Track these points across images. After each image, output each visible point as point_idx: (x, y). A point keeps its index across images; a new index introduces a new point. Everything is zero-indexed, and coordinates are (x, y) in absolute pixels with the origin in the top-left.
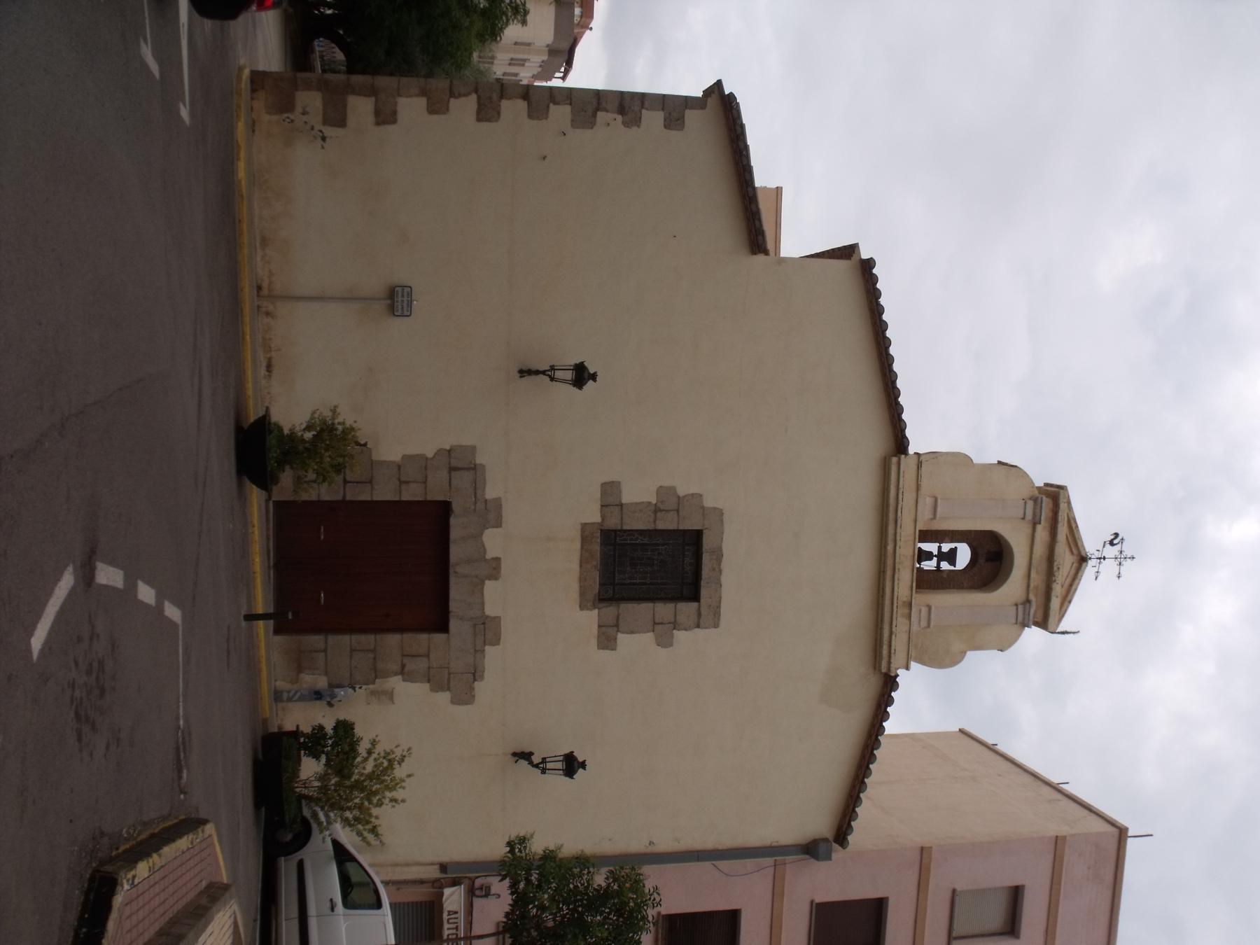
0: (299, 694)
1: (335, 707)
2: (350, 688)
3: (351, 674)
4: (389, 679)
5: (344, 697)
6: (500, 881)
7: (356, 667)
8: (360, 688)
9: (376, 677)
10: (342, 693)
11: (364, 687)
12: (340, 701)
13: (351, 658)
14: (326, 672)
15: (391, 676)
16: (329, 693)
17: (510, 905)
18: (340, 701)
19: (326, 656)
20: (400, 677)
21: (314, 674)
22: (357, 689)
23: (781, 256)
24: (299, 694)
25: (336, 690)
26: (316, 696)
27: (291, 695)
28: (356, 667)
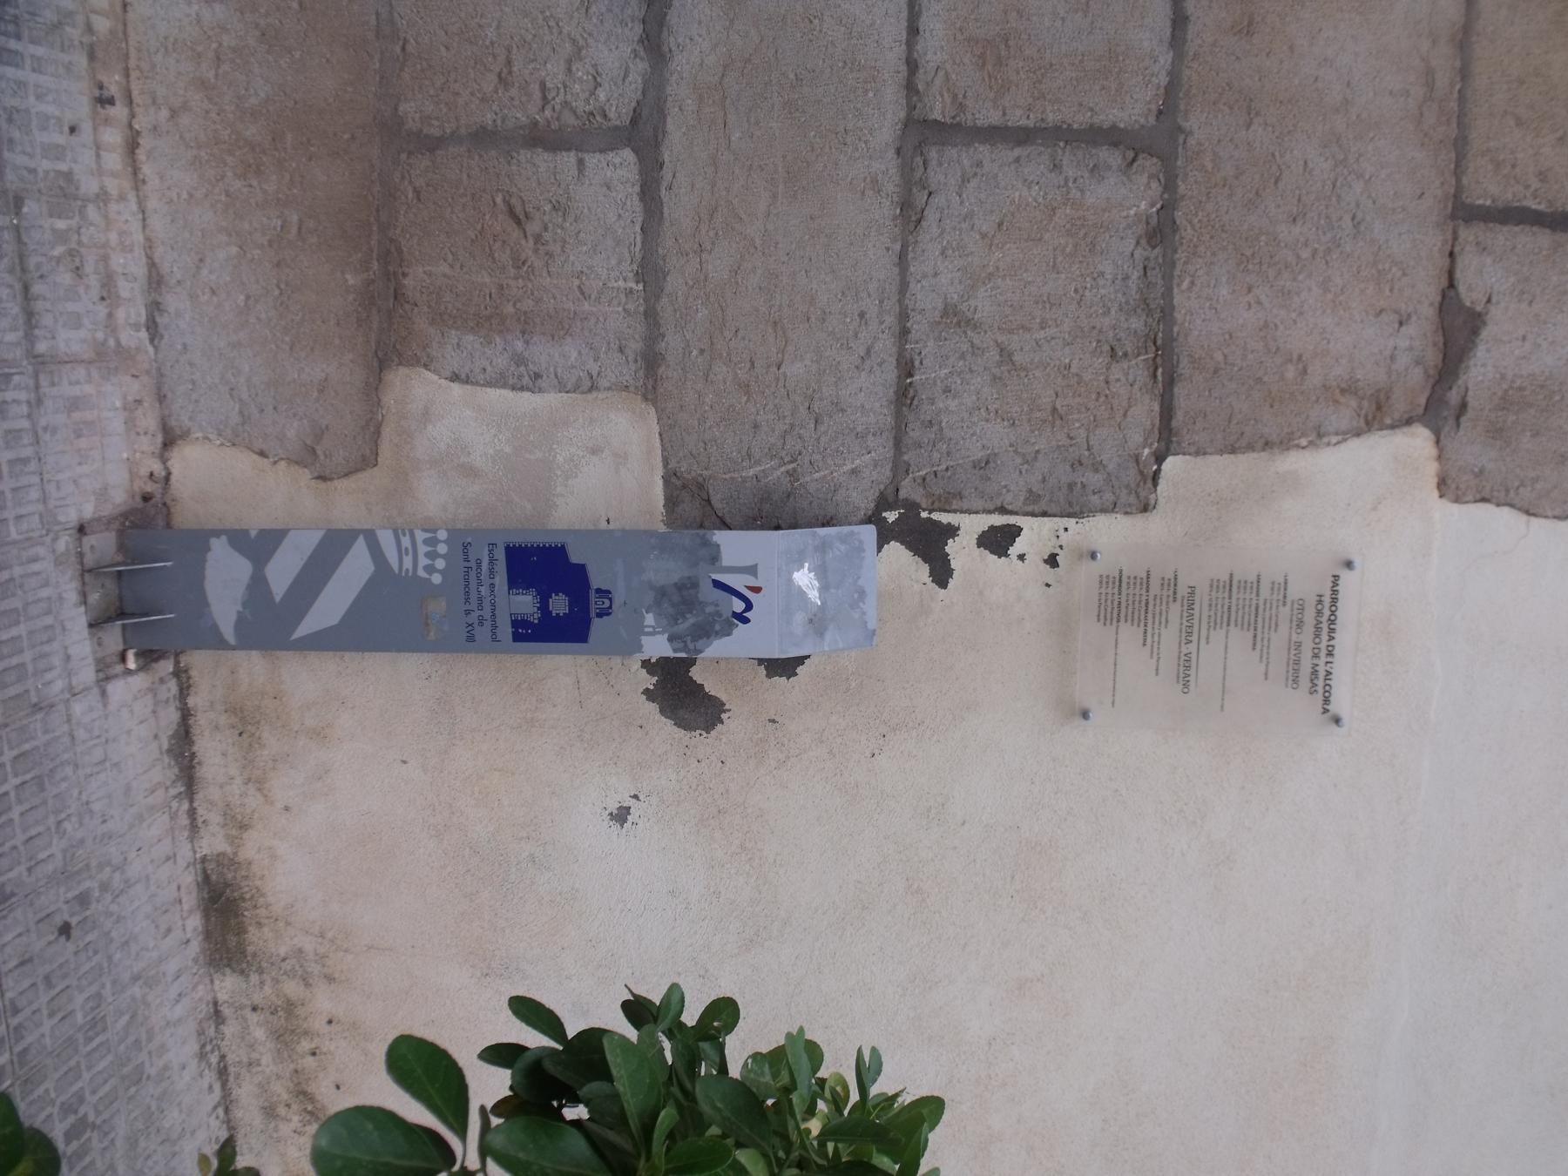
0: (356, 569)
1: (734, 725)
2: (886, 535)
3: (904, 396)
4: (1294, 461)
5: (818, 623)
6: (860, 1051)
7: (954, 317)
8: (998, 541)
9: (1167, 440)
10: (804, 578)
11: (1035, 534)
12: (783, 667)
13: (910, 216)
14: (651, 361)
15: (1319, 436)
16: (666, 570)
17: (867, 1070)
18: (783, 667)
19: (649, 192)
20: (1418, 441)
21: (533, 382)
22: (962, 552)
23: (508, 1072)
24: (356, 569)
25: (735, 546)
26: (526, 603)
27: (282, 572)
28: (954, 317)
